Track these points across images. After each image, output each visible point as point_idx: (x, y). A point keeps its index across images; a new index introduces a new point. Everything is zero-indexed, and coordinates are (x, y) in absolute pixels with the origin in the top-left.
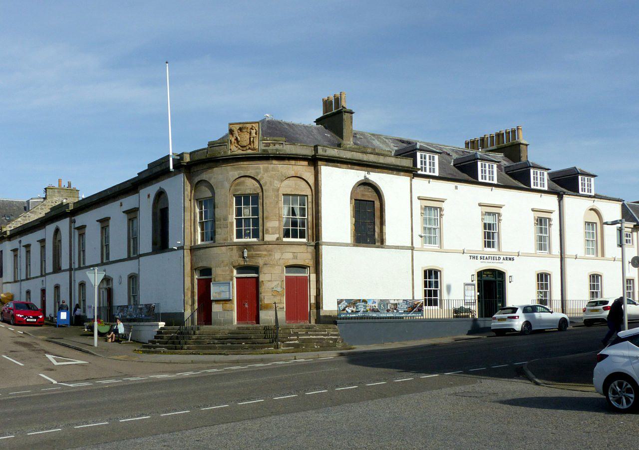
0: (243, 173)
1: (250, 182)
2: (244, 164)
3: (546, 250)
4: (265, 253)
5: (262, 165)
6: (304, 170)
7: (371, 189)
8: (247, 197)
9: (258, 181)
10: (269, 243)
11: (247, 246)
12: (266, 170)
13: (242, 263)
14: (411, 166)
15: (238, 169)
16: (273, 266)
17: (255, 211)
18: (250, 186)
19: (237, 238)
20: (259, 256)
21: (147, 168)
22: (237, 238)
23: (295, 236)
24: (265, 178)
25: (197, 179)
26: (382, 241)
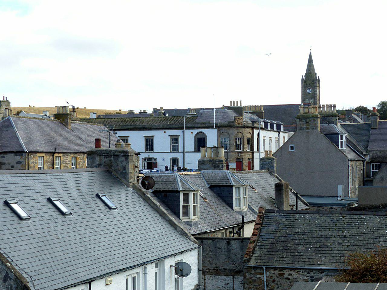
0: (239, 131)
1: (240, 134)
2: (239, 129)
3: (293, 149)
4: (244, 155)
5: (244, 129)
6: (250, 130)
7: (199, 134)
8: (239, 139)
9: (242, 134)
10: (245, 152)
11: (240, 152)
12: (244, 131)
13: (238, 157)
14: (3, 99)
15: (238, 130)
16: (246, 158)
17: (241, 143)
18: (240, 135)
19: (291, 149)
20: (243, 155)
21: (151, 113)
22: (291, 149)
23: (150, 150)
24: (244, 133)
25: (222, 131)
26: (152, 150)
